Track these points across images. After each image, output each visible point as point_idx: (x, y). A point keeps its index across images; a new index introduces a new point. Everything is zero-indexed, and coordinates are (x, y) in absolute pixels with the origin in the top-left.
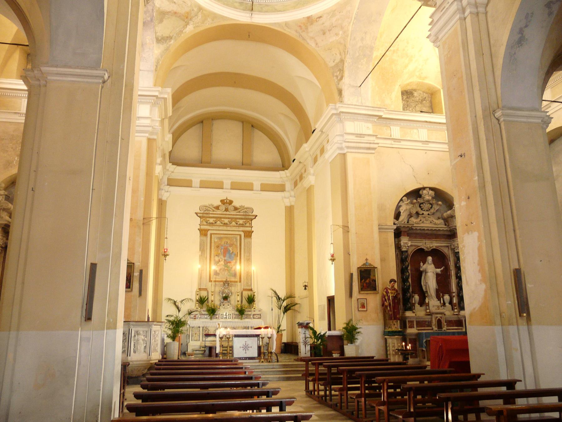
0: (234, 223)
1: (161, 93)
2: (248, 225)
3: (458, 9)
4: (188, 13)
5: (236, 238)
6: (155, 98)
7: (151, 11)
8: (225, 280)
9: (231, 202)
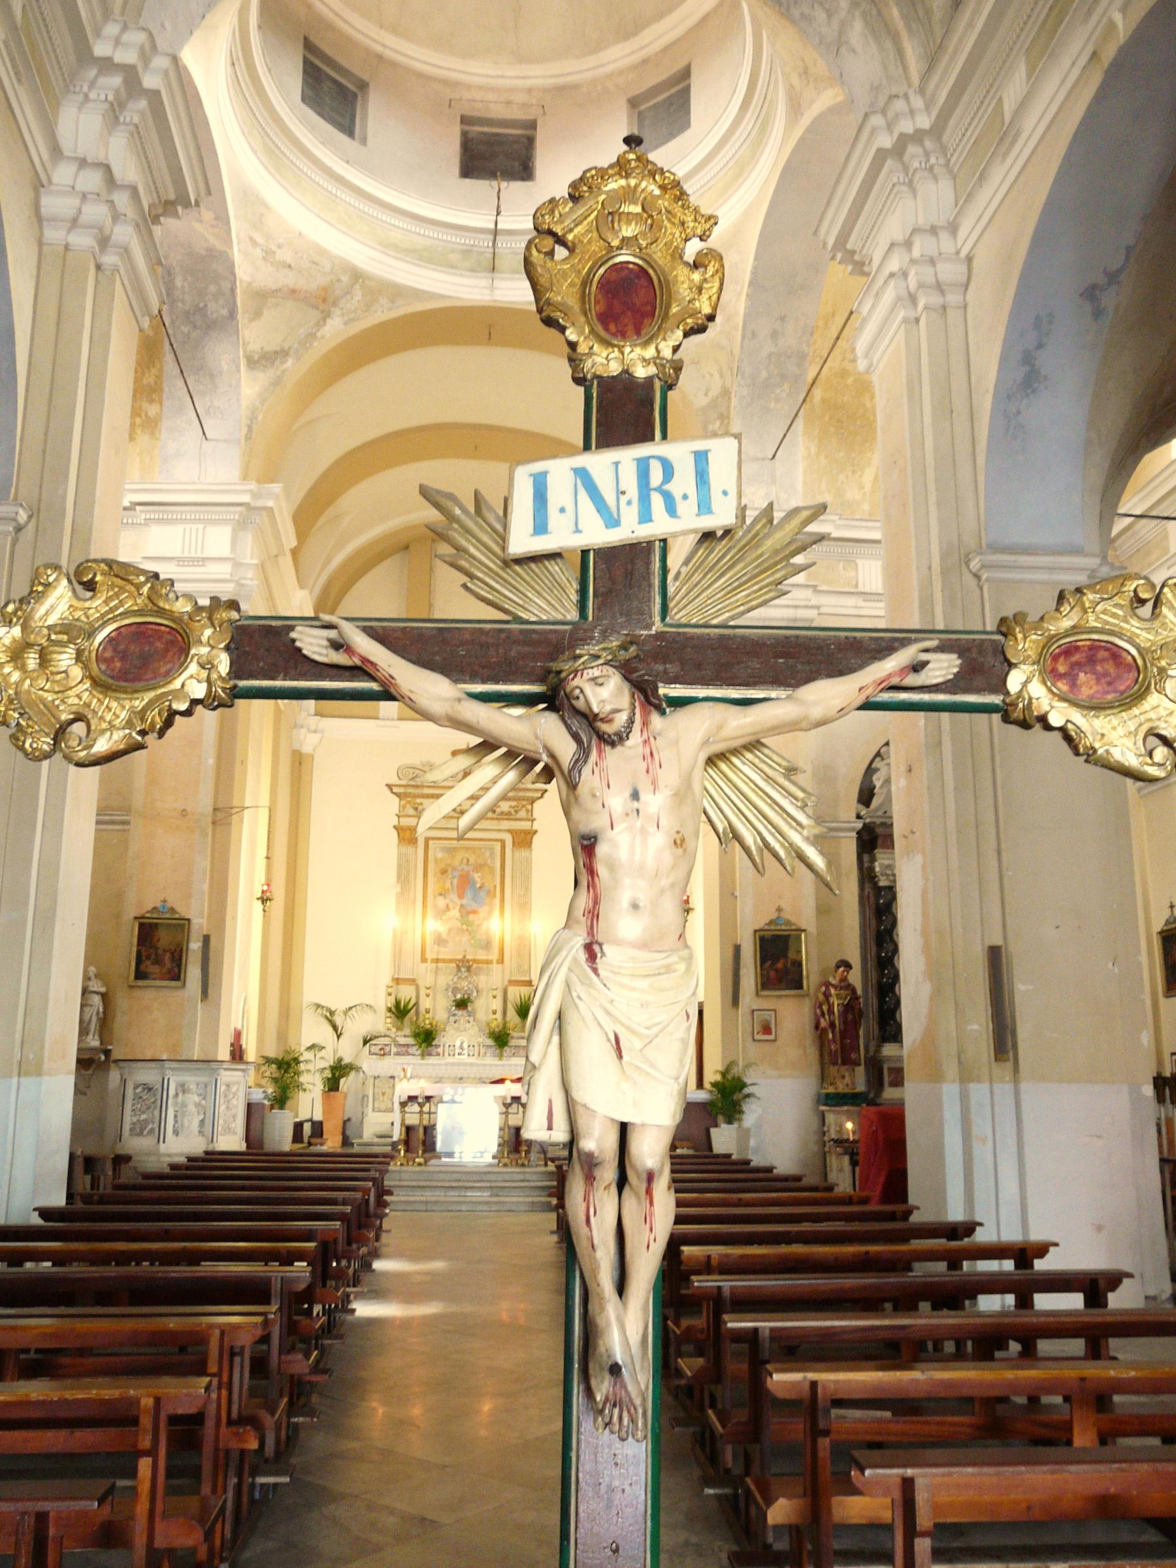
1: (256, 495)
2: (522, 814)
3: (899, 299)
4: (325, 289)
5: (492, 849)
6: (240, 509)
7: (228, 293)
8: (460, 957)
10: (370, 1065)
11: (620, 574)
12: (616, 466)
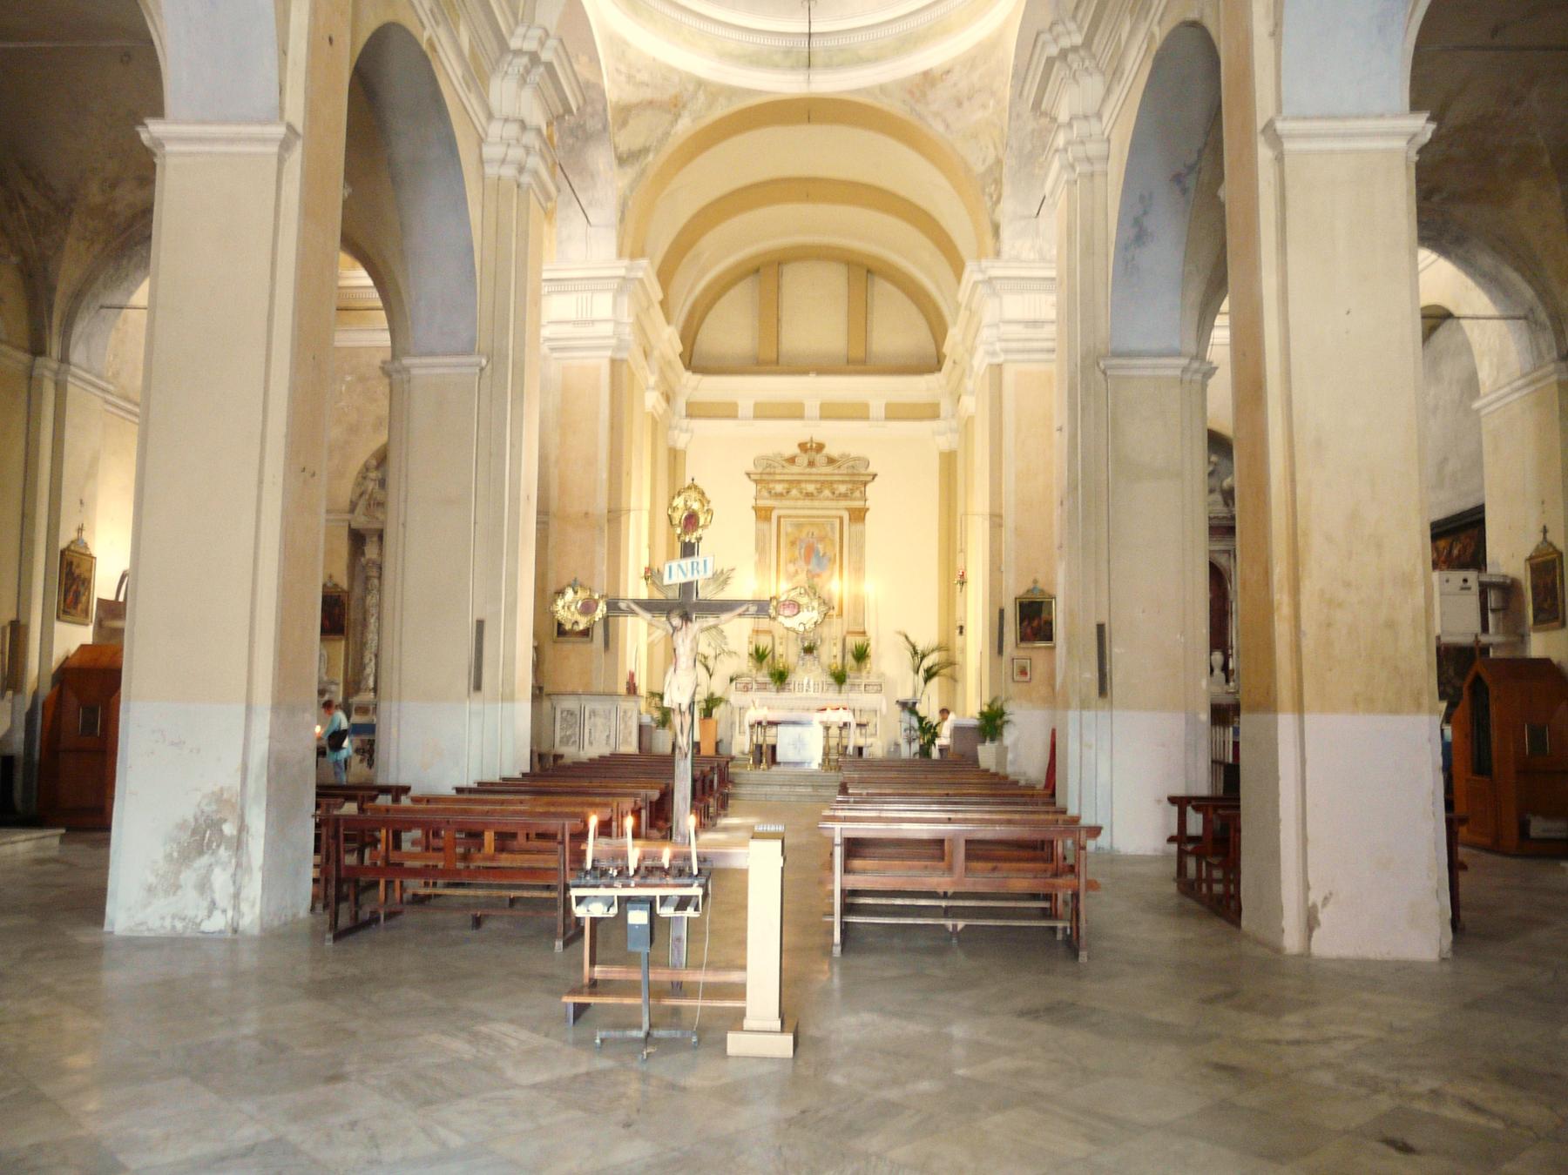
0: (827, 493)
1: (628, 269)
2: (857, 494)
3: (1062, 167)
5: (832, 525)
9: (820, 447)
10: (736, 698)
11: (687, 588)
12: (686, 563)
